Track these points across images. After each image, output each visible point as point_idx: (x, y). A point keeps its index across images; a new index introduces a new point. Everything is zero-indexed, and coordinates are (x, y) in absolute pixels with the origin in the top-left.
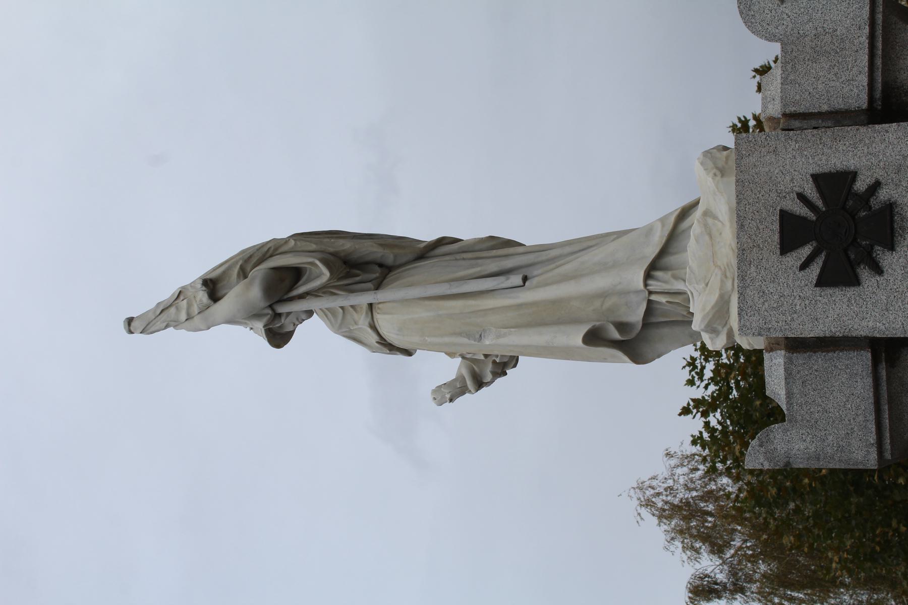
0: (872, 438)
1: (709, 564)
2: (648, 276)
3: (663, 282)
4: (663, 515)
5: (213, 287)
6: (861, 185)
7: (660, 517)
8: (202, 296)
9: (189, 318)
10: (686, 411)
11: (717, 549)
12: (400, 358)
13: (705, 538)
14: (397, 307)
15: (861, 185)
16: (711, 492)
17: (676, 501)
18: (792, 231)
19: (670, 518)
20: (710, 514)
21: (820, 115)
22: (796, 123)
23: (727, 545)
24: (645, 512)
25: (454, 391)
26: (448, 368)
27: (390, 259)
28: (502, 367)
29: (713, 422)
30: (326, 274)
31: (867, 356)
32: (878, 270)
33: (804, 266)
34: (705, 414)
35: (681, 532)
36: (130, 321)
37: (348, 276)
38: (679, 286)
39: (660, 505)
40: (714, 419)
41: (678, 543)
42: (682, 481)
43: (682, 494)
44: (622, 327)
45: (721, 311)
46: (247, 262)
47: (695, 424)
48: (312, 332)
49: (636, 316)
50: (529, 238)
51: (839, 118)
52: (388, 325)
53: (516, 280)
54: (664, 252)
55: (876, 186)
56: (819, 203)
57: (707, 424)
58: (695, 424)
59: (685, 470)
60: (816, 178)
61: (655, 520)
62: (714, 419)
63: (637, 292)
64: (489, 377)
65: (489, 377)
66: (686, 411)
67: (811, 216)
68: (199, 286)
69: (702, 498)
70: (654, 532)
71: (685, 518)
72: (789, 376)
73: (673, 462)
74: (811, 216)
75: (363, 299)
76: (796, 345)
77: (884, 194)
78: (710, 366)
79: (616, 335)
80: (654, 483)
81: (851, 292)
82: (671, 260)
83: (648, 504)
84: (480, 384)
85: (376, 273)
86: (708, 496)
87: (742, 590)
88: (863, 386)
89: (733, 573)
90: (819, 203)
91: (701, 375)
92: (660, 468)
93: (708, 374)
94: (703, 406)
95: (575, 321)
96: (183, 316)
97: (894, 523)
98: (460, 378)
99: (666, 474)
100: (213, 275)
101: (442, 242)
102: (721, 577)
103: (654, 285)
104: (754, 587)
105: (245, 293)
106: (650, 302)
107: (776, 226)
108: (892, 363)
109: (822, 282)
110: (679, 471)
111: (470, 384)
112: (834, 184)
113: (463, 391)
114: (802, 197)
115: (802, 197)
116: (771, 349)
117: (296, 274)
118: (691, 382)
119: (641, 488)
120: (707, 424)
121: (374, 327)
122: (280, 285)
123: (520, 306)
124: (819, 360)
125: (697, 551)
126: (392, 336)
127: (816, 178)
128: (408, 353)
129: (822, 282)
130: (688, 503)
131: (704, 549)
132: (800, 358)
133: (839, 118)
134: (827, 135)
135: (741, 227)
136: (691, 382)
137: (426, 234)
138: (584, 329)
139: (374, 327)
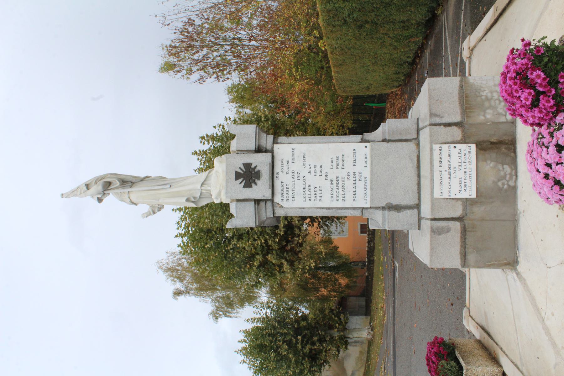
0: (254, 221)
1: (179, 286)
2: (201, 186)
3: (206, 187)
4: (165, 271)
5: (88, 186)
6: (253, 166)
7: (164, 272)
8: (85, 188)
9: (80, 194)
10: (176, 236)
11: (181, 281)
12: (134, 206)
13: (178, 278)
14: (136, 193)
15: (253, 166)
16: (180, 264)
17: (169, 267)
18: (238, 176)
19: (167, 271)
20: (179, 270)
21: (244, 151)
22: (239, 152)
23: (185, 279)
24: (159, 270)
25: (148, 214)
26: (145, 208)
27: (134, 181)
28: (160, 208)
29: (185, 240)
30: (118, 184)
31: (254, 203)
32: (256, 184)
33: (240, 183)
34: (182, 237)
35: (171, 276)
36: (62, 194)
37: (123, 184)
38: (209, 188)
39: (164, 268)
40: (185, 239)
41: (169, 279)
42: (171, 260)
43: (171, 265)
44: (194, 198)
45: (219, 194)
46: (97, 180)
47: (179, 241)
48: (111, 198)
49: (198, 195)
50: (169, 176)
51: (249, 151)
52: (133, 197)
53: (168, 186)
54: (205, 181)
55: (256, 167)
56: (244, 170)
57: (183, 241)
58: (179, 241)
59: (172, 257)
60: (244, 164)
61: (162, 273)
62: (185, 239)
63: (198, 190)
64: (156, 211)
65: (156, 211)
66: (176, 236)
67: (242, 172)
68: (84, 185)
69: (177, 266)
70: (163, 276)
71: (172, 272)
72: (236, 207)
73: (168, 255)
74: (242, 172)
75: (127, 190)
76: (238, 200)
77: (257, 169)
78: (184, 224)
79: (193, 200)
80: (162, 261)
81: (250, 189)
82: (206, 182)
83: (160, 268)
84: (154, 213)
85: (130, 184)
86: (180, 265)
87: (189, 293)
88: (253, 209)
89: (186, 287)
90: (244, 170)
91: (181, 227)
92: (164, 256)
93: (183, 226)
94: (182, 236)
95: (183, 196)
96: (79, 193)
97: (236, 268)
98: (150, 212)
99: (166, 258)
100: (87, 183)
101: (147, 177)
102: (183, 289)
103: (203, 188)
104: (193, 292)
105: (97, 188)
106: (201, 192)
107: (235, 175)
108: (258, 204)
109: (244, 187)
110: (170, 257)
111: (152, 213)
112: (247, 166)
113: (150, 214)
114: (240, 168)
115: (240, 168)
116: (231, 202)
117: (110, 183)
118: (178, 229)
119: (158, 262)
120: (183, 241)
121: (129, 198)
122: (107, 185)
123: (169, 193)
124: (243, 204)
125: (175, 281)
126: (134, 200)
127: (244, 164)
128: (136, 204)
129: (244, 187)
130: (172, 267)
131: (178, 281)
132: (239, 203)
133: (249, 151)
134: (246, 155)
135: (227, 174)
136: (178, 229)
137: (143, 176)
138: (186, 198)
139: (129, 198)
